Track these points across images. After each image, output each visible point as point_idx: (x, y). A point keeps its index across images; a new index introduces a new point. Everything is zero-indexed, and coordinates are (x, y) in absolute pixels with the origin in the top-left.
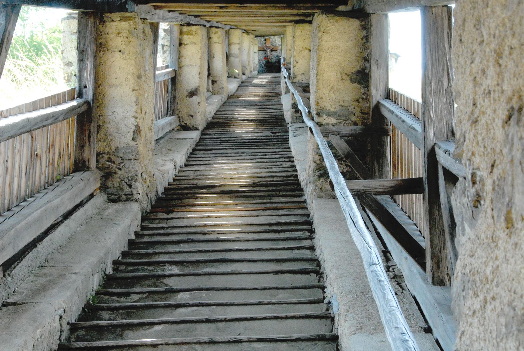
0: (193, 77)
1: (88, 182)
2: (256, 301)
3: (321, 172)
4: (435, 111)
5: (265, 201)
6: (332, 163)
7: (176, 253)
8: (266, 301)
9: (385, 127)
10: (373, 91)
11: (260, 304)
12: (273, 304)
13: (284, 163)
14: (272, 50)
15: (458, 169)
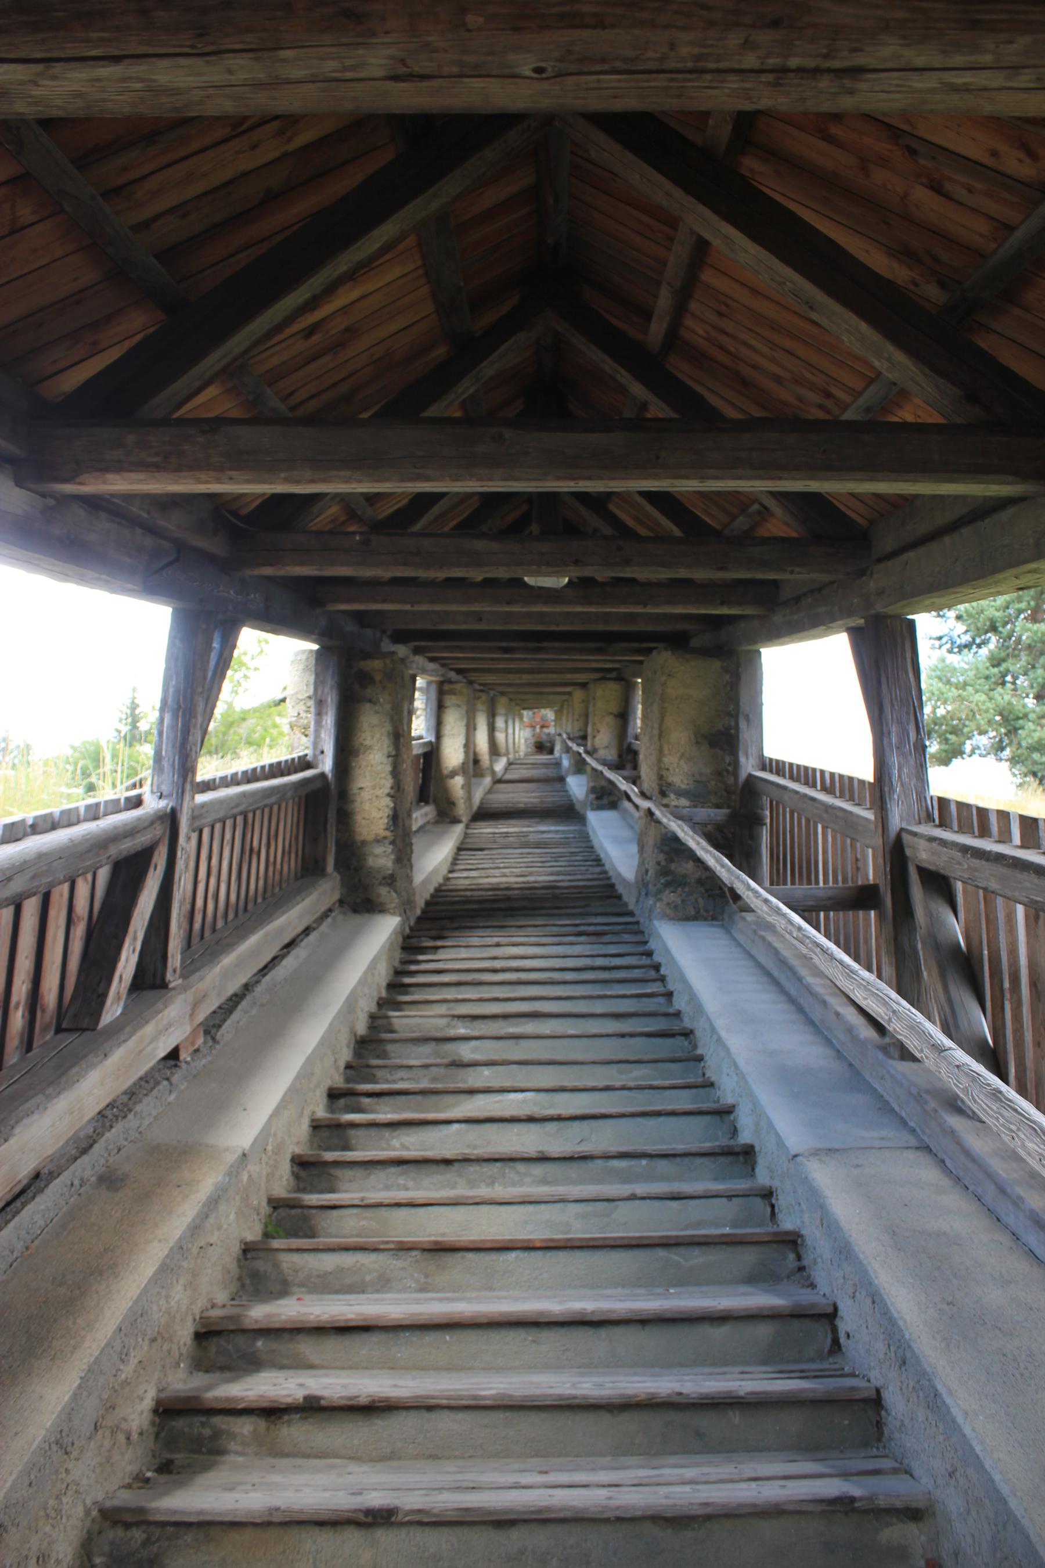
0: (453, 754)
1: (325, 892)
2: (601, 1084)
3: (669, 878)
4: (900, 777)
5: (577, 922)
6: (718, 861)
7: (457, 1001)
8: (618, 1084)
9: (760, 811)
10: (742, 760)
11: (607, 1089)
12: (630, 1089)
13: (591, 869)
14: (542, 727)
15: (970, 867)
